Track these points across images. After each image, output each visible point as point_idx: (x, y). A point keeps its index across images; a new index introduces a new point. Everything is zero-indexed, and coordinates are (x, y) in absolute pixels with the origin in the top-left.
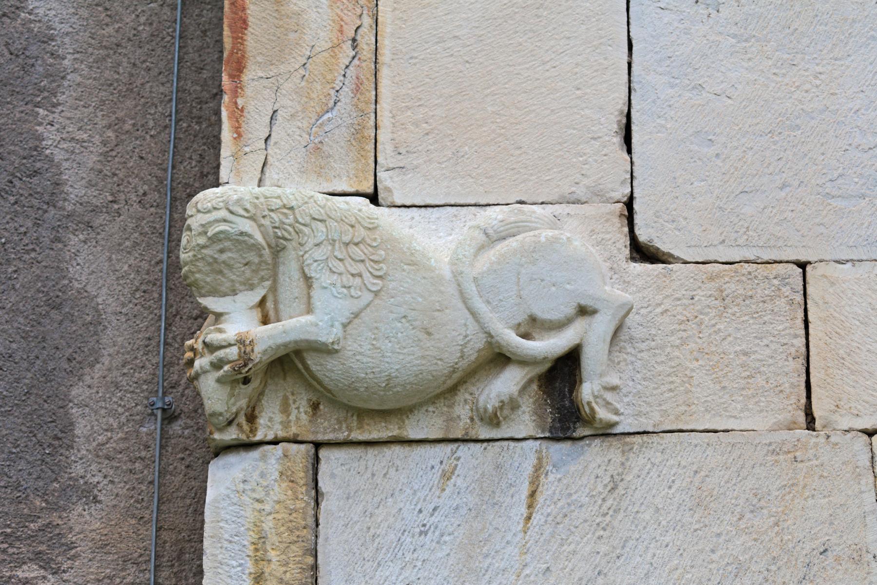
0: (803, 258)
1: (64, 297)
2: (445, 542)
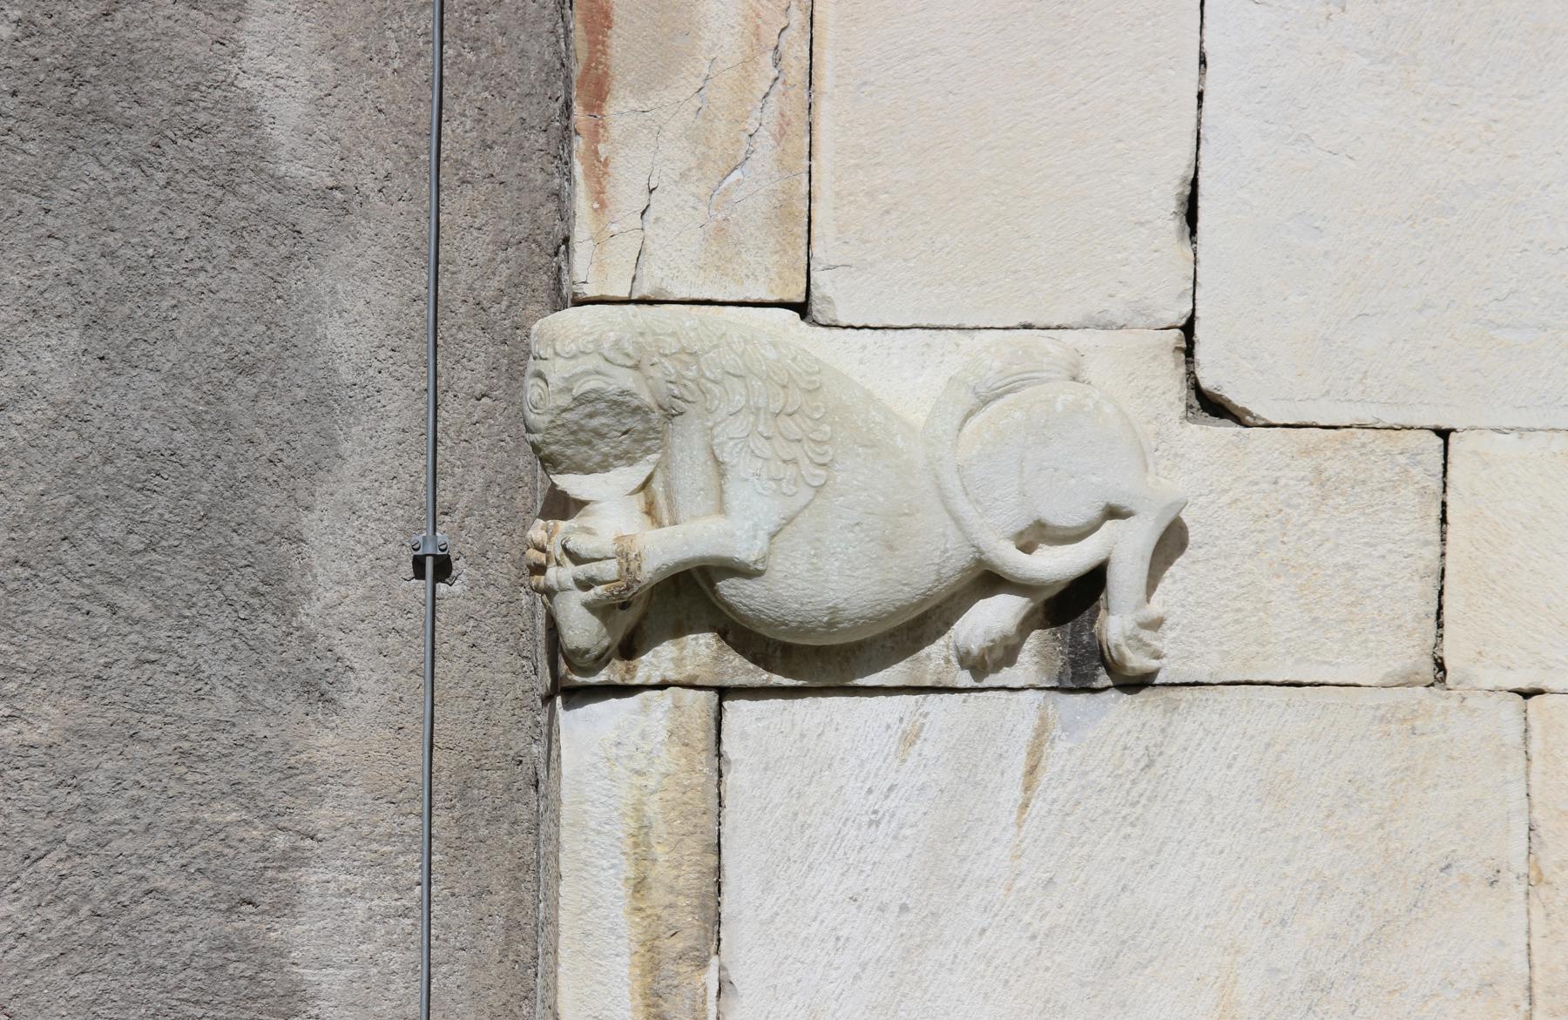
0: (1445, 425)
1: (259, 355)
2: (905, 838)
